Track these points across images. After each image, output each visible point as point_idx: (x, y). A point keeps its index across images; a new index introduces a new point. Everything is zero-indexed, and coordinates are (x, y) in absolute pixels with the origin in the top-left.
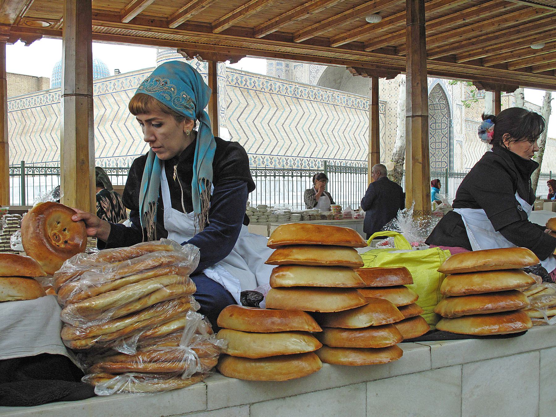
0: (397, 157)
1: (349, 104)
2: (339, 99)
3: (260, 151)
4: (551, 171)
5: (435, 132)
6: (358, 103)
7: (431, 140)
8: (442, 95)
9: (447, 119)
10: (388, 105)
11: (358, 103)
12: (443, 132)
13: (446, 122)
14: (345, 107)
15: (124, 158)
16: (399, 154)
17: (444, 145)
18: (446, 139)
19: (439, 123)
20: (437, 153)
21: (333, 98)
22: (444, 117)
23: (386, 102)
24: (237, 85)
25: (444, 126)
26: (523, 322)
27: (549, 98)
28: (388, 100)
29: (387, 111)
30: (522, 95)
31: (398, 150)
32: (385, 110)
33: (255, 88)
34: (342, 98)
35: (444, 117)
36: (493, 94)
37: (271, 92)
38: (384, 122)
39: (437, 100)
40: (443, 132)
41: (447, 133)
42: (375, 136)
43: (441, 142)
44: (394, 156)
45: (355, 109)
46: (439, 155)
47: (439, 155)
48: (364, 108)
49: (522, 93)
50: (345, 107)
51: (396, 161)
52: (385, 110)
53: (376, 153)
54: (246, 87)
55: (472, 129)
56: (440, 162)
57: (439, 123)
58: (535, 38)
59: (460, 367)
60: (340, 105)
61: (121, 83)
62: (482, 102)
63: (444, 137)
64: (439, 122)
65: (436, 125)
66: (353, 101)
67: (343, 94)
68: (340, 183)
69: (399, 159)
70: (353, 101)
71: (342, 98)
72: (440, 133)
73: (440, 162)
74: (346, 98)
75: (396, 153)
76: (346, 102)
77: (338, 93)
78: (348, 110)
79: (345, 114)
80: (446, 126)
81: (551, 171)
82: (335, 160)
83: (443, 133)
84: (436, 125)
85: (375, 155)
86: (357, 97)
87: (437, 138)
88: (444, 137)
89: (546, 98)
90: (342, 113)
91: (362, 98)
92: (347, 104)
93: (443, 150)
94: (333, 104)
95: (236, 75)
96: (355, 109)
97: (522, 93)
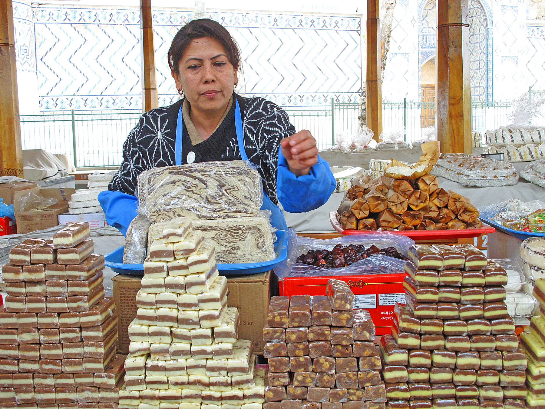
3: (84, 91)
4: (405, 99)
7: (484, 46)
12: (481, 47)
13: (484, 33)
15: (314, 95)
17: (482, 64)
20: (475, 75)
24: (67, 21)
25: (482, 37)
26: (407, 253)
33: (97, 22)
37: (126, 22)
41: (485, 47)
43: (479, 60)
46: (477, 78)
47: (477, 78)
54: (82, 21)
56: (478, 87)
59: (184, 277)
61: (311, 21)
72: (478, 49)
73: (478, 87)
80: (483, 37)
81: (405, 99)
87: (475, 55)
93: (481, 70)
95: (64, 11)
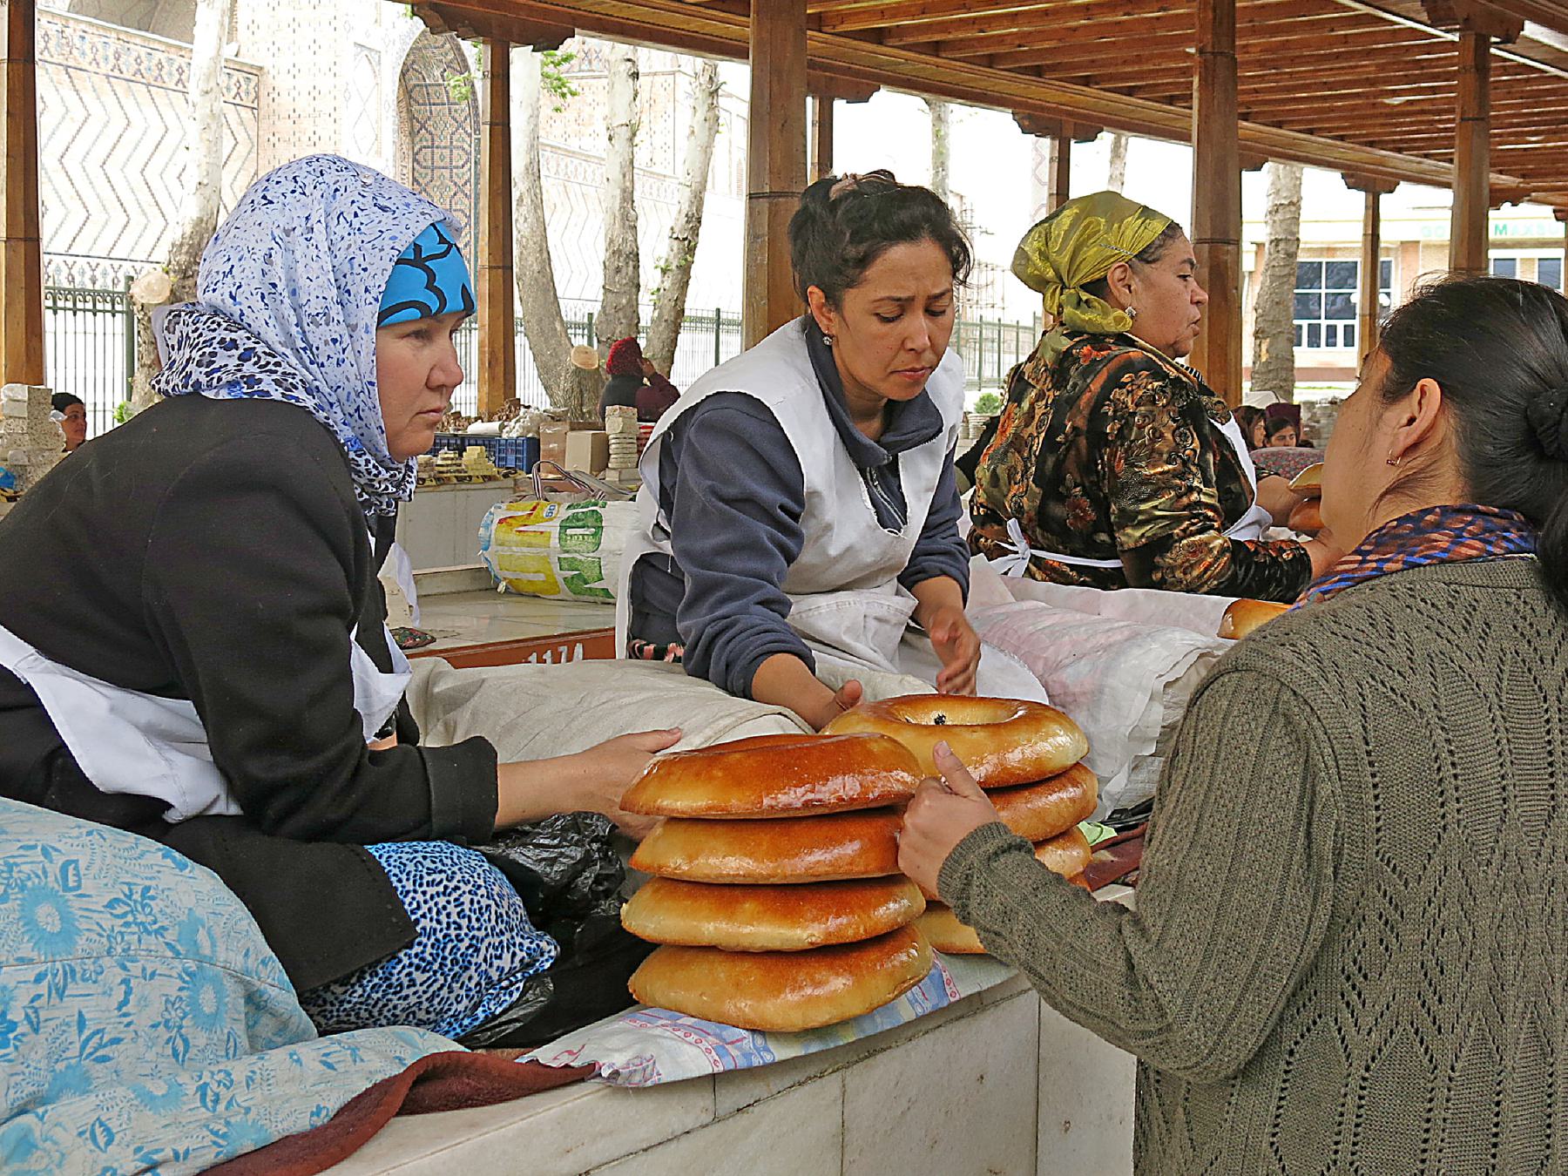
0: (183, 258)
1: (124, 68)
2: (87, 47)
4: (718, 310)
5: (429, 178)
6: (160, 66)
8: (451, 56)
9: (470, 135)
10: (268, 80)
11: (160, 66)
13: (466, 146)
14: (108, 76)
16: (191, 246)
18: (467, 202)
19: (445, 148)
21: (64, 41)
22: (461, 131)
23: (261, 68)
27: (711, 78)
28: (267, 66)
29: (264, 100)
30: (629, 64)
31: (188, 231)
32: (257, 97)
34: (100, 46)
35: (461, 131)
36: (1053, 145)
38: (253, 134)
39: (437, 73)
40: (455, 179)
41: (469, 180)
42: (20, 177)
44: (175, 256)
45: (148, 85)
48: (180, 85)
49: (629, 60)
50: (108, 76)
51: (180, 270)
52: (257, 97)
53: (26, 240)
55: (557, 172)
57: (445, 148)
58: (1093, 61)
60: (88, 68)
62: (593, 89)
63: (460, 195)
64: (443, 144)
65: (433, 153)
66: (139, 57)
67: (102, 32)
68: (90, 337)
69: (190, 262)
70: (139, 57)
71: (100, 46)
74: (114, 45)
75: (182, 245)
76: (112, 61)
77: (83, 26)
78: (120, 86)
79: (110, 100)
80: (465, 157)
82: (70, 260)
83: (456, 180)
84: (433, 153)
85: (21, 247)
86: (156, 46)
88: (460, 195)
89: (702, 80)
90: (98, 98)
91: (173, 50)
92: (116, 67)
94: (65, 63)
96: (148, 85)
97: (629, 60)
